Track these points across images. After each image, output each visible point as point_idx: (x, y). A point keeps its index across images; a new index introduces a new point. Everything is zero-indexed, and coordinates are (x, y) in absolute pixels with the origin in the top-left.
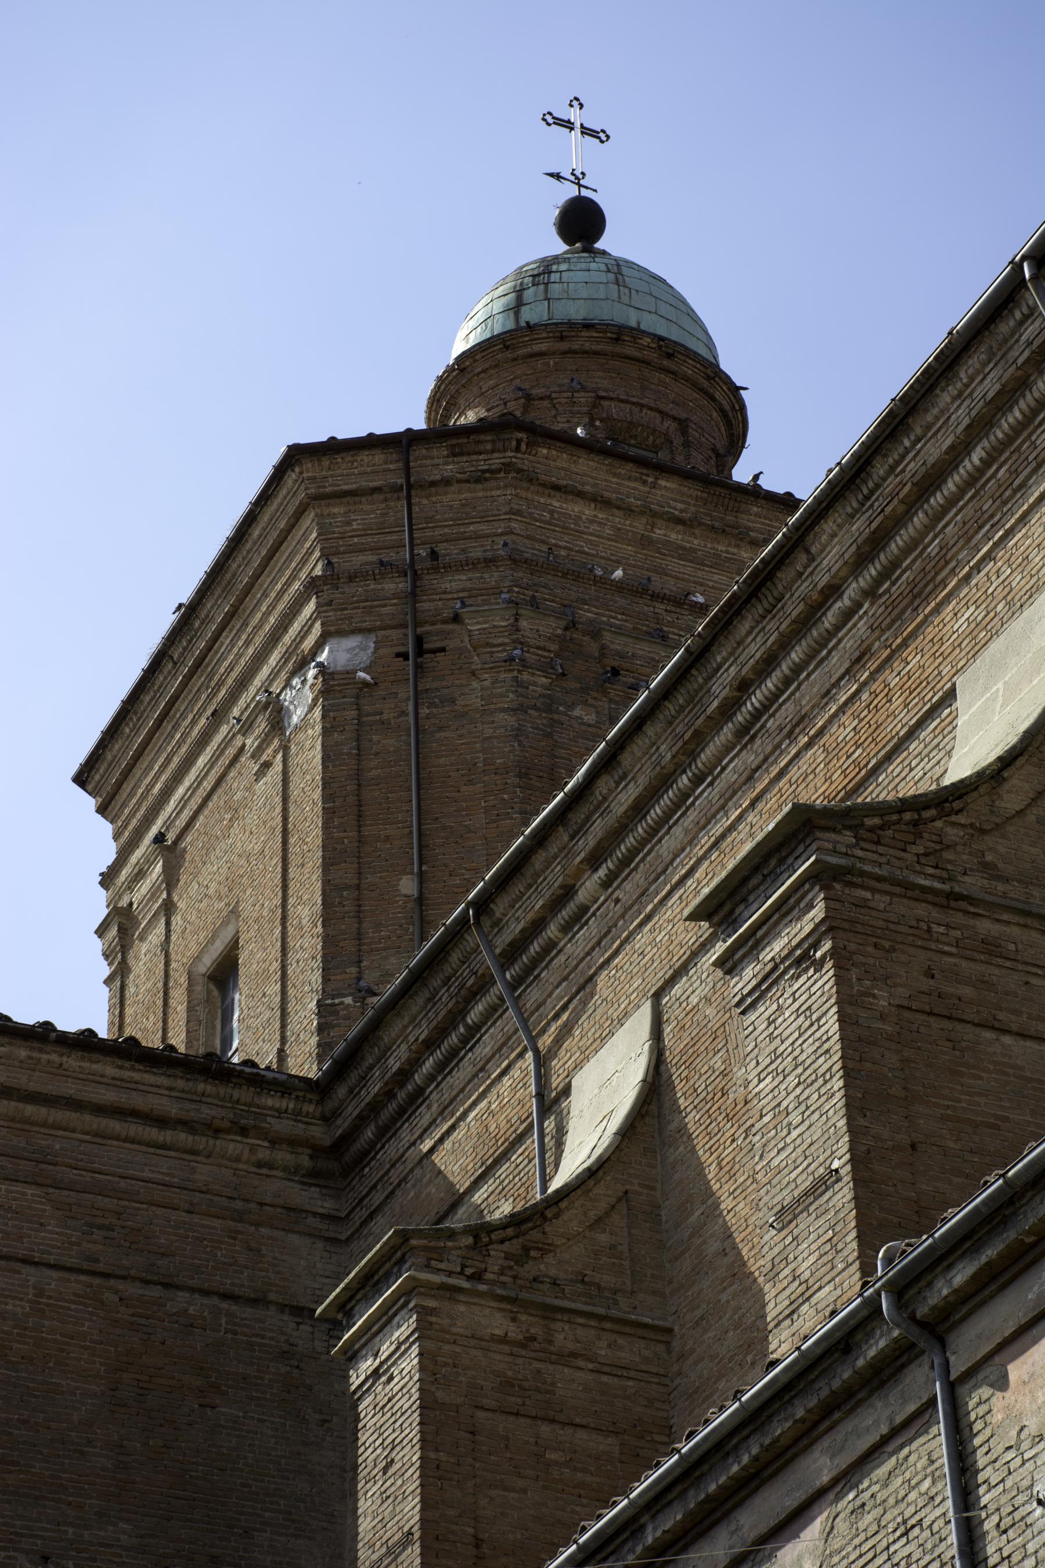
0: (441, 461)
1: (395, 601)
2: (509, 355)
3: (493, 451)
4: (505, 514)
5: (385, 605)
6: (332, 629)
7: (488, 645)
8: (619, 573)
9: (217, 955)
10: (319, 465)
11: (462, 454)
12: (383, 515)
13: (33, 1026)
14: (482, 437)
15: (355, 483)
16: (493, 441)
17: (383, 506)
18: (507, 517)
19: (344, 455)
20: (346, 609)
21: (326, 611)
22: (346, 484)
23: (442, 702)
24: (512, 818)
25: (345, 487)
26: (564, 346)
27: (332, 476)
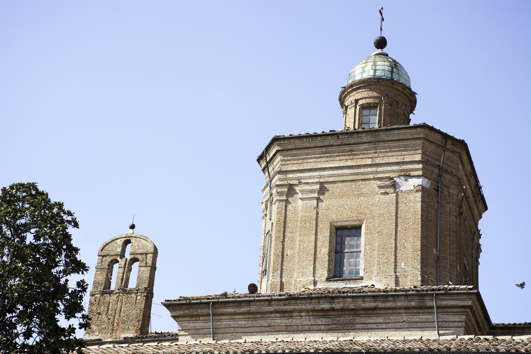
2: (391, 85)
26: (403, 91)
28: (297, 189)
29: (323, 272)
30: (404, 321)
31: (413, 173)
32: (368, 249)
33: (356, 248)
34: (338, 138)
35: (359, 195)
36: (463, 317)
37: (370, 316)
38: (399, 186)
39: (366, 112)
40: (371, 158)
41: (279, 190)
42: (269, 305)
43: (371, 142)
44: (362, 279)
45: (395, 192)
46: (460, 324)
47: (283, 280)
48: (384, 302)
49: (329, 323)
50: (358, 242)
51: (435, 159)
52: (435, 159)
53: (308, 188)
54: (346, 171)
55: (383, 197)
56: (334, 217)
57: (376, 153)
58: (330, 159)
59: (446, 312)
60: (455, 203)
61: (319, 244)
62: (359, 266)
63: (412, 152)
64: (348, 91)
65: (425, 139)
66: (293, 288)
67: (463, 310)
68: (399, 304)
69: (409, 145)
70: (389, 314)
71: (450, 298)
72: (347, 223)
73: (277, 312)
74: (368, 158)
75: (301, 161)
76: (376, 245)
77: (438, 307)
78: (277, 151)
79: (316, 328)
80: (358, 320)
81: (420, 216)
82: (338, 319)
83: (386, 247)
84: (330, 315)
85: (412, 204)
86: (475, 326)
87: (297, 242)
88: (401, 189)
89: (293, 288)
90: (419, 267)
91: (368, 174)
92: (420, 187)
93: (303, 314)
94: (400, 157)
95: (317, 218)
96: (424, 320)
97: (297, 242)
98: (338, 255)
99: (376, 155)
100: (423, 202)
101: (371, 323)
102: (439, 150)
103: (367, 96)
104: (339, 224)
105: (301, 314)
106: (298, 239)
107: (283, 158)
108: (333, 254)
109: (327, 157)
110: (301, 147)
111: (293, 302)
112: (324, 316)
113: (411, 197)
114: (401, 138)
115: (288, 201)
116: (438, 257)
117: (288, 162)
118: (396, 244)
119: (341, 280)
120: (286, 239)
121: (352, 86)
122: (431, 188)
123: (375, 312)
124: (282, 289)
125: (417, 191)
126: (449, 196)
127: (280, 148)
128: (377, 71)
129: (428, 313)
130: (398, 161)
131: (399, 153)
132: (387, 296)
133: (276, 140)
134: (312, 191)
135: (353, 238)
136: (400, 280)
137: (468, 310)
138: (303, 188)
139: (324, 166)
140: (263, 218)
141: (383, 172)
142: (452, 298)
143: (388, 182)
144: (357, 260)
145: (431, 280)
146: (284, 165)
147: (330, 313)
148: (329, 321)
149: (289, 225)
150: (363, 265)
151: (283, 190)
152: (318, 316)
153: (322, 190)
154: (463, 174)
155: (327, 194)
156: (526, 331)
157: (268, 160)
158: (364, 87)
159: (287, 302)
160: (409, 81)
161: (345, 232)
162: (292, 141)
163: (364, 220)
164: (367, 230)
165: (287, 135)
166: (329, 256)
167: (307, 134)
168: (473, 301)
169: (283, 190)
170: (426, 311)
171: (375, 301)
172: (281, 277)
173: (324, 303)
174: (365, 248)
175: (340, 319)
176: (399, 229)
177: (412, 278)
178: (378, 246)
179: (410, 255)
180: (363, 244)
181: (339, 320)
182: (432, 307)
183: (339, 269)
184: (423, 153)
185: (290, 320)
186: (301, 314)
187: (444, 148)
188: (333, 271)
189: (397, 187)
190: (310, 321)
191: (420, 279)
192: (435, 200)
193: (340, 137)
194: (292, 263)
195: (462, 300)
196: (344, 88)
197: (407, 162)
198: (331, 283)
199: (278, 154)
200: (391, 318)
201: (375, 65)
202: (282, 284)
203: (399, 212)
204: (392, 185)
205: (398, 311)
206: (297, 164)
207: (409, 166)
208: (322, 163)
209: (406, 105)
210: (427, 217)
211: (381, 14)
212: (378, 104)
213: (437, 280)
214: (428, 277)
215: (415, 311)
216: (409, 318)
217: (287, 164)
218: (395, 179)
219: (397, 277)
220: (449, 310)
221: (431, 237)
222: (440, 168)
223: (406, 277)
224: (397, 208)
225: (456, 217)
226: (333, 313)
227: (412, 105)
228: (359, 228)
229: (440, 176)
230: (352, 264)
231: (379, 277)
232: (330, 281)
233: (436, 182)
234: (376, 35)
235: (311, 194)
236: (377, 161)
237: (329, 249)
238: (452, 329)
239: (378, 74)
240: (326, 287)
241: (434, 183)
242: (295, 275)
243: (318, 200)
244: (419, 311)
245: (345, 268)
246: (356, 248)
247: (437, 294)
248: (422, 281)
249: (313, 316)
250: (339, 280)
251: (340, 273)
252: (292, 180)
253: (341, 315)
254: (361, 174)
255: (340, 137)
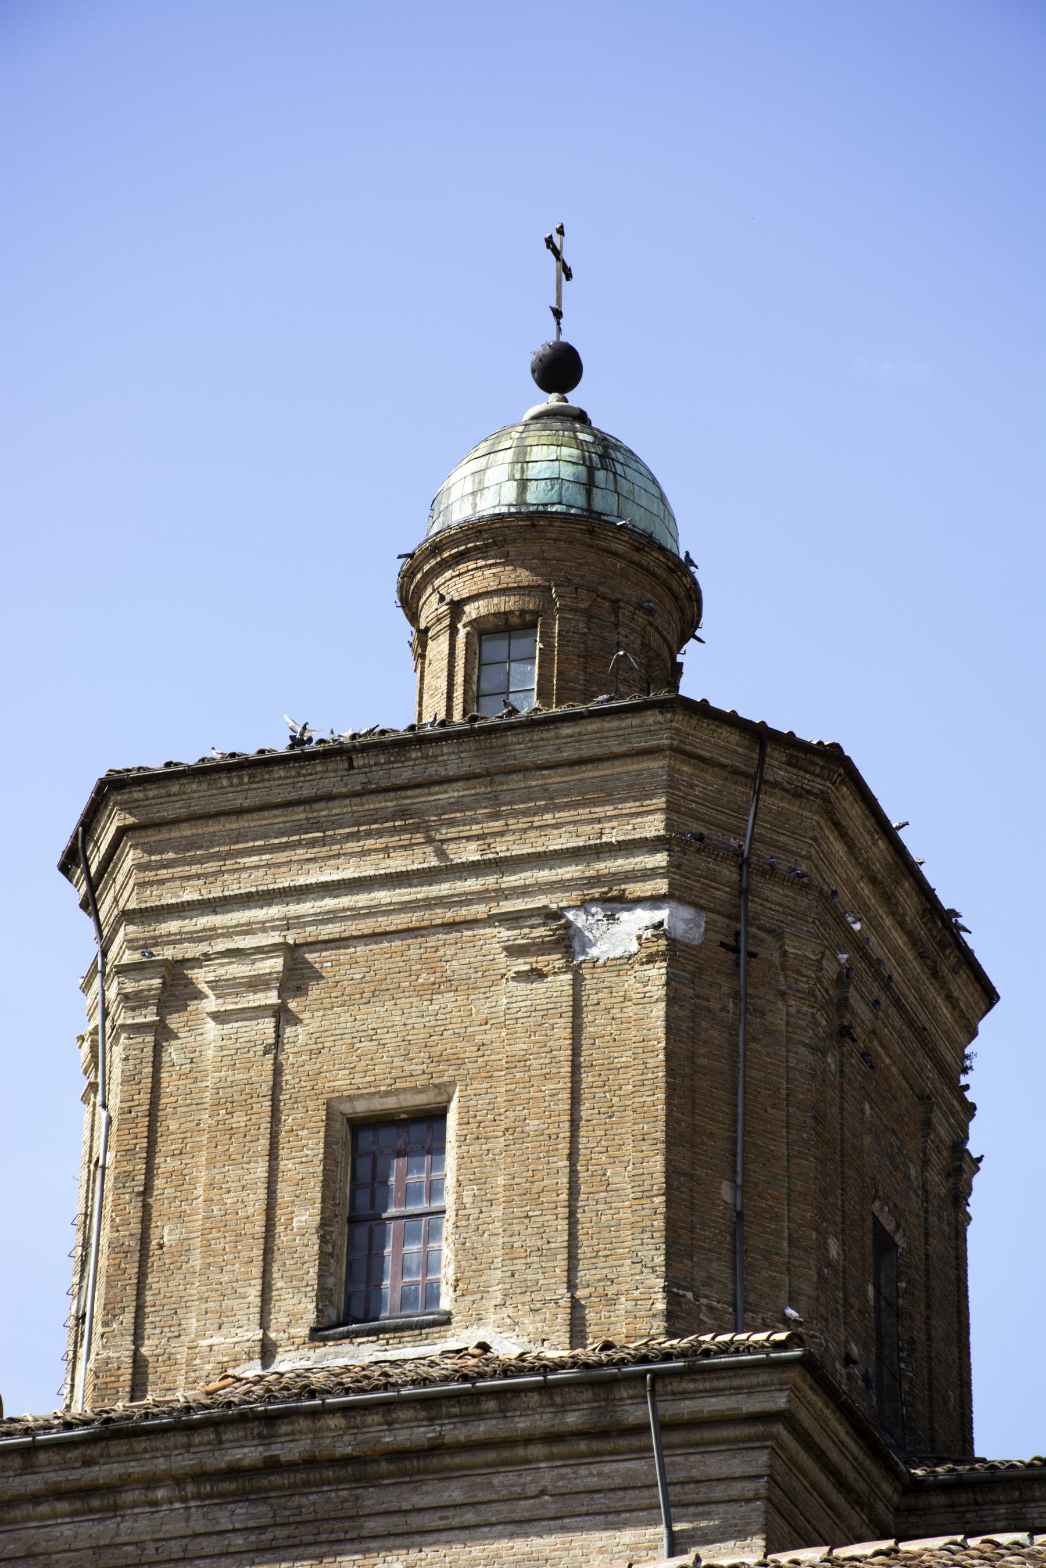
0: (776, 763)
1: (728, 889)
2: (587, 538)
3: (818, 776)
4: (810, 838)
5: (719, 889)
6: (677, 893)
7: (798, 972)
8: (857, 927)
9: (379, 1108)
10: (688, 721)
11: (795, 766)
12: (719, 791)
13: (1031, 1465)
14: (817, 760)
15: (710, 752)
16: (822, 767)
17: (721, 782)
18: (811, 842)
19: (711, 722)
20: (689, 878)
21: (674, 873)
22: (702, 749)
23: (755, 1011)
24: (808, 1160)
25: (702, 753)
26: (636, 556)
27: (693, 736)
28: (201, 976)
29: (298, 1306)
30: (543, 1492)
31: (636, 889)
32: (467, 1200)
33: (430, 1200)
34: (351, 767)
35: (435, 988)
36: (761, 1460)
37: (414, 1478)
38: (587, 944)
39: (496, 648)
40: (478, 837)
41: (130, 987)
42: (28, 1468)
43: (475, 776)
44: (448, 1322)
45: (567, 969)
46: (749, 1488)
47: (144, 1351)
48: (465, 1418)
49: (263, 1521)
50: (435, 1175)
51: (725, 828)
52: (725, 828)
53: (238, 970)
54: (383, 896)
55: (523, 988)
56: (340, 1082)
57: (495, 816)
58: (324, 851)
59: (697, 1444)
60: (812, 993)
61: (284, 1192)
62: (438, 1269)
63: (631, 807)
64: (426, 568)
65: (677, 751)
66: (181, 1380)
67: (758, 1429)
68: (522, 1424)
69: (617, 777)
70: (487, 1465)
71: (707, 1385)
72: (390, 1103)
73: (57, 1494)
74: (468, 838)
75: (212, 866)
76: (501, 1181)
77: (666, 1426)
78: (122, 832)
79: (210, 1545)
80: (372, 1498)
81: (662, 1057)
82: (297, 1500)
83: (536, 1187)
84: (266, 1490)
85: (631, 1011)
86: (828, 1486)
87: (200, 1191)
88: (594, 952)
89: (181, 1380)
90: (660, 1260)
91: (469, 902)
92: (663, 942)
93: (160, 1494)
94: (587, 829)
95: (276, 1088)
96: (618, 1481)
97: (200, 1191)
98: (362, 1232)
99: (497, 825)
100: (672, 1000)
101: (420, 1510)
102: (741, 791)
103: (493, 586)
104: (361, 1107)
105: (151, 1496)
106: (203, 1178)
107: (146, 858)
108: (340, 1230)
109: (313, 843)
110: (213, 809)
111: (118, 1447)
112: (240, 1496)
113: (630, 983)
114: (585, 753)
115: (166, 1027)
116: (740, 1215)
117: (164, 873)
118: (573, 1174)
119: (368, 1333)
120: (159, 1183)
121: (435, 548)
122: (706, 941)
123: (435, 1462)
124: (138, 1389)
125: (651, 959)
126: (784, 969)
127: (130, 820)
128: (532, 485)
129: (632, 1451)
130: (580, 842)
131: (583, 812)
132: (475, 1396)
133: (113, 787)
134: (256, 984)
135: (418, 1159)
136: (590, 1316)
137: (779, 1429)
138: (221, 971)
139: (301, 881)
140: (85, 1099)
141: (523, 891)
142: (716, 1384)
143: (541, 931)
144: (434, 1245)
145: (710, 1308)
146: (151, 883)
147: (264, 1482)
148: (263, 1513)
149: (170, 1124)
150: (452, 1266)
151: (144, 984)
152: (221, 1495)
153: (297, 976)
154: (856, 873)
155: (315, 991)
156: (1037, 1493)
157: (93, 870)
158: (481, 552)
159: (94, 1451)
160: (668, 516)
161: (388, 1137)
162: (175, 788)
163: (453, 1083)
164: (463, 1123)
165: (156, 764)
166: (323, 1240)
167: (233, 755)
168: (795, 1390)
169: (144, 984)
170: (622, 1443)
171: (431, 1420)
172: (138, 1337)
173: (238, 1443)
174: (459, 1197)
175: (304, 1500)
176: (586, 1111)
177: (633, 1312)
178: (508, 1187)
179: (626, 1215)
180: (450, 1182)
181: (300, 1507)
182: (642, 1429)
183: (362, 1287)
184: (670, 809)
185: (111, 1524)
186: (151, 1496)
187: (758, 781)
188: (339, 1298)
189: (576, 945)
190: (188, 1519)
191: (661, 1306)
192: (726, 987)
193: (359, 761)
194: (178, 1277)
195: (751, 1390)
196: (411, 556)
197: (609, 844)
198: (330, 1348)
199: (127, 843)
200: (496, 1481)
201: (522, 460)
202: (139, 1364)
203: (586, 1043)
204: (557, 942)
205: (520, 1452)
206: (198, 876)
207: (620, 862)
208: (295, 867)
209: (650, 612)
210: (692, 1058)
211: (557, 253)
212: (536, 613)
213: (734, 1306)
214: (697, 1297)
215: (583, 1446)
216: (562, 1477)
217: (162, 882)
218: (570, 915)
219: (576, 1307)
220: (709, 1434)
221: (711, 1136)
222: (741, 861)
223: (611, 1301)
224: (577, 1028)
225: (814, 1049)
226: (276, 1480)
227: (682, 612)
228: (436, 1116)
229: (743, 892)
230: (414, 1261)
231: (510, 1310)
232: (325, 1340)
233: (729, 917)
234: (542, 336)
235: (251, 996)
236: (502, 848)
237: (323, 1210)
238: (722, 1508)
239: (535, 495)
240: (308, 1364)
241: (722, 921)
242: (193, 1323)
243: (282, 1016)
244: (596, 1445)
245: (387, 1283)
246: (430, 1200)
247: (657, 1375)
248: (670, 1315)
249: (198, 1497)
250: (357, 1334)
251: (368, 1300)
252: (180, 942)
253: (306, 1484)
254: (442, 902)
255: (359, 761)
